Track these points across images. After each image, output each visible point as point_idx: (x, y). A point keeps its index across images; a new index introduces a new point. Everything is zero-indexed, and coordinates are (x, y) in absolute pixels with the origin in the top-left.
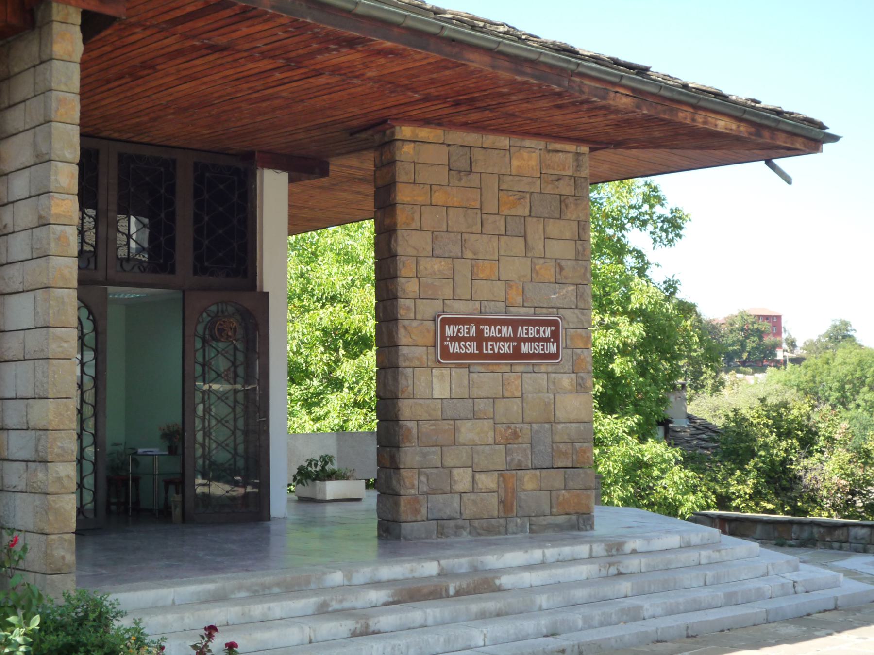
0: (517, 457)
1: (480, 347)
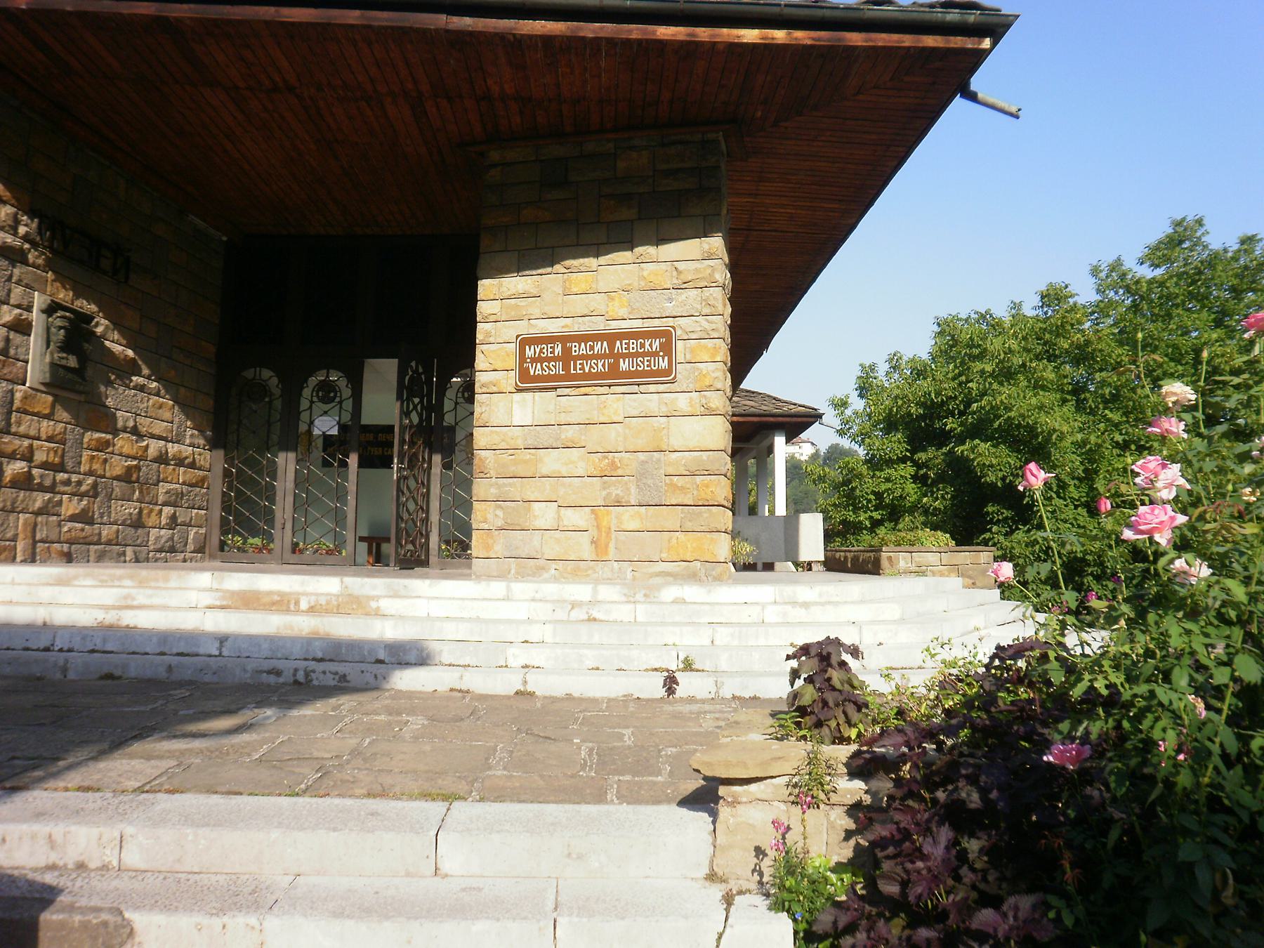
0: (616, 491)
1: (566, 367)
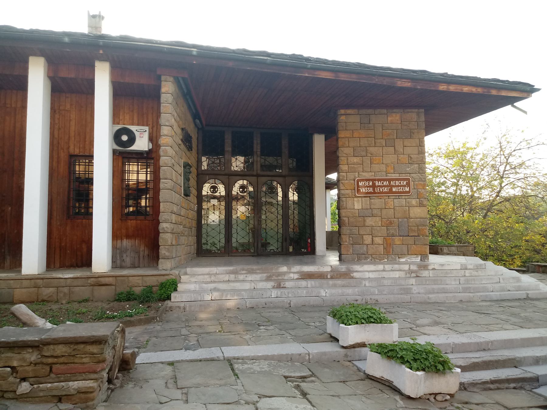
0: (392, 231)
1: (374, 190)
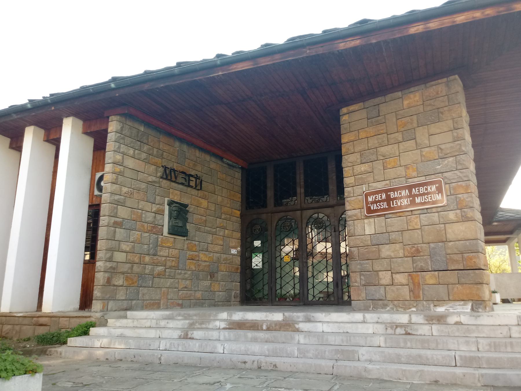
0: (421, 264)
1: (389, 204)
